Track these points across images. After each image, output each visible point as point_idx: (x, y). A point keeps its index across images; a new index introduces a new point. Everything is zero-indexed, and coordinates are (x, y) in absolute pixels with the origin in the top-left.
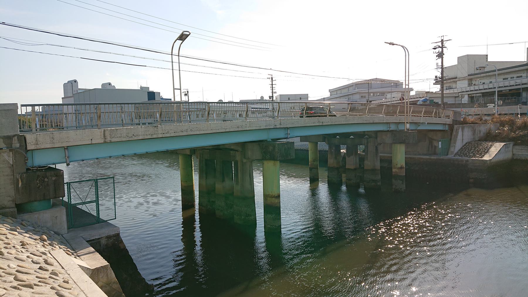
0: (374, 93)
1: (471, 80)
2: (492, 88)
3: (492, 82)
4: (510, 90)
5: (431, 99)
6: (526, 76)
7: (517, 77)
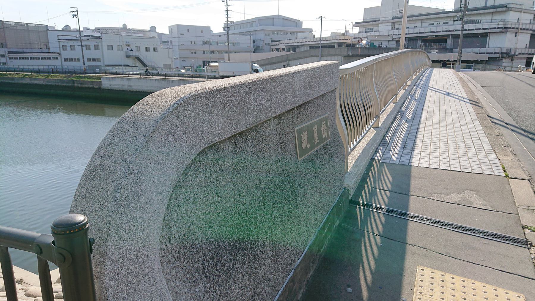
0: (277, 31)
1: (394, 23)
2: (481, 29)
3: (416, 27)
4: (436, 36)
5: (372, 42)
6: (491, 19)
7: (444, 23)
